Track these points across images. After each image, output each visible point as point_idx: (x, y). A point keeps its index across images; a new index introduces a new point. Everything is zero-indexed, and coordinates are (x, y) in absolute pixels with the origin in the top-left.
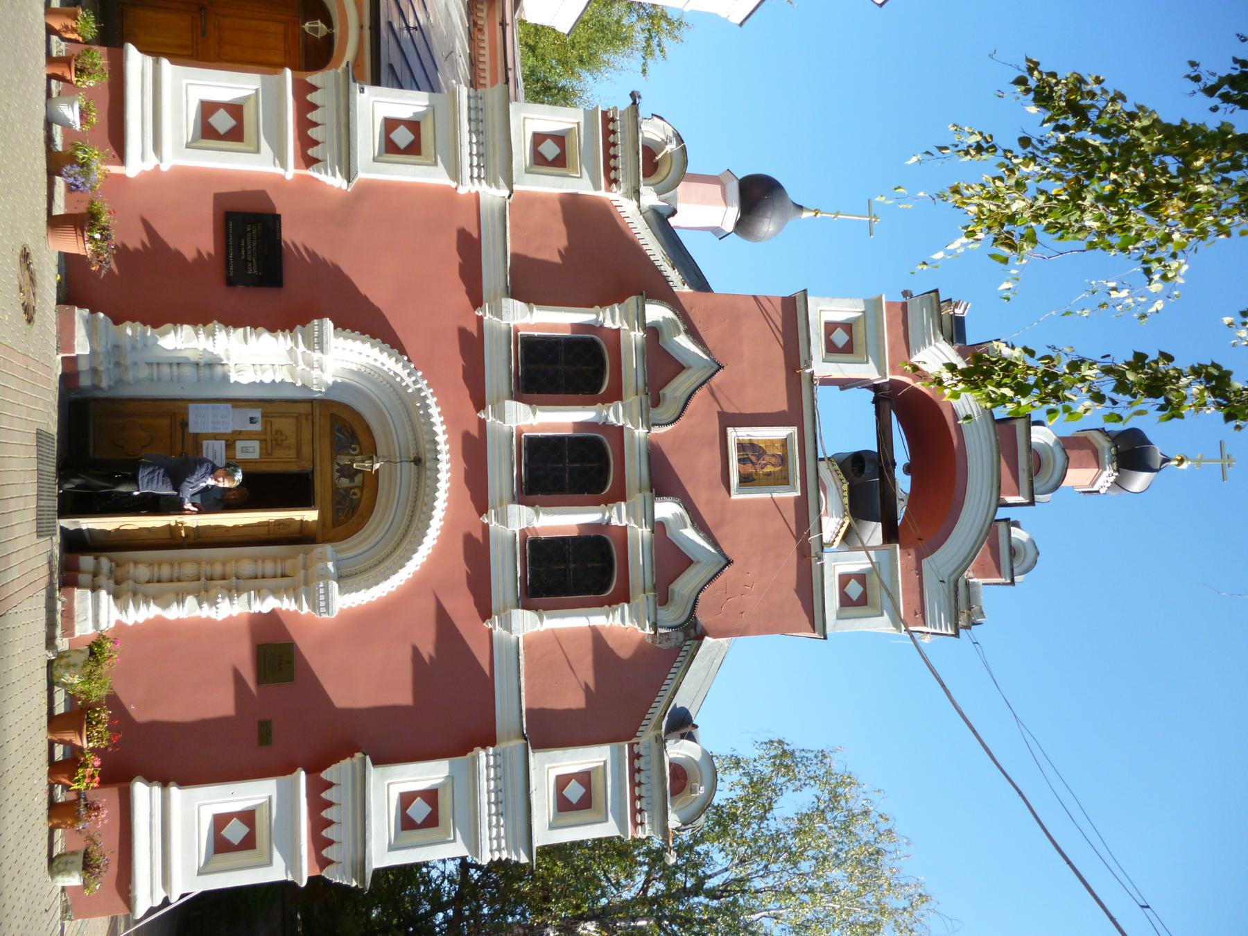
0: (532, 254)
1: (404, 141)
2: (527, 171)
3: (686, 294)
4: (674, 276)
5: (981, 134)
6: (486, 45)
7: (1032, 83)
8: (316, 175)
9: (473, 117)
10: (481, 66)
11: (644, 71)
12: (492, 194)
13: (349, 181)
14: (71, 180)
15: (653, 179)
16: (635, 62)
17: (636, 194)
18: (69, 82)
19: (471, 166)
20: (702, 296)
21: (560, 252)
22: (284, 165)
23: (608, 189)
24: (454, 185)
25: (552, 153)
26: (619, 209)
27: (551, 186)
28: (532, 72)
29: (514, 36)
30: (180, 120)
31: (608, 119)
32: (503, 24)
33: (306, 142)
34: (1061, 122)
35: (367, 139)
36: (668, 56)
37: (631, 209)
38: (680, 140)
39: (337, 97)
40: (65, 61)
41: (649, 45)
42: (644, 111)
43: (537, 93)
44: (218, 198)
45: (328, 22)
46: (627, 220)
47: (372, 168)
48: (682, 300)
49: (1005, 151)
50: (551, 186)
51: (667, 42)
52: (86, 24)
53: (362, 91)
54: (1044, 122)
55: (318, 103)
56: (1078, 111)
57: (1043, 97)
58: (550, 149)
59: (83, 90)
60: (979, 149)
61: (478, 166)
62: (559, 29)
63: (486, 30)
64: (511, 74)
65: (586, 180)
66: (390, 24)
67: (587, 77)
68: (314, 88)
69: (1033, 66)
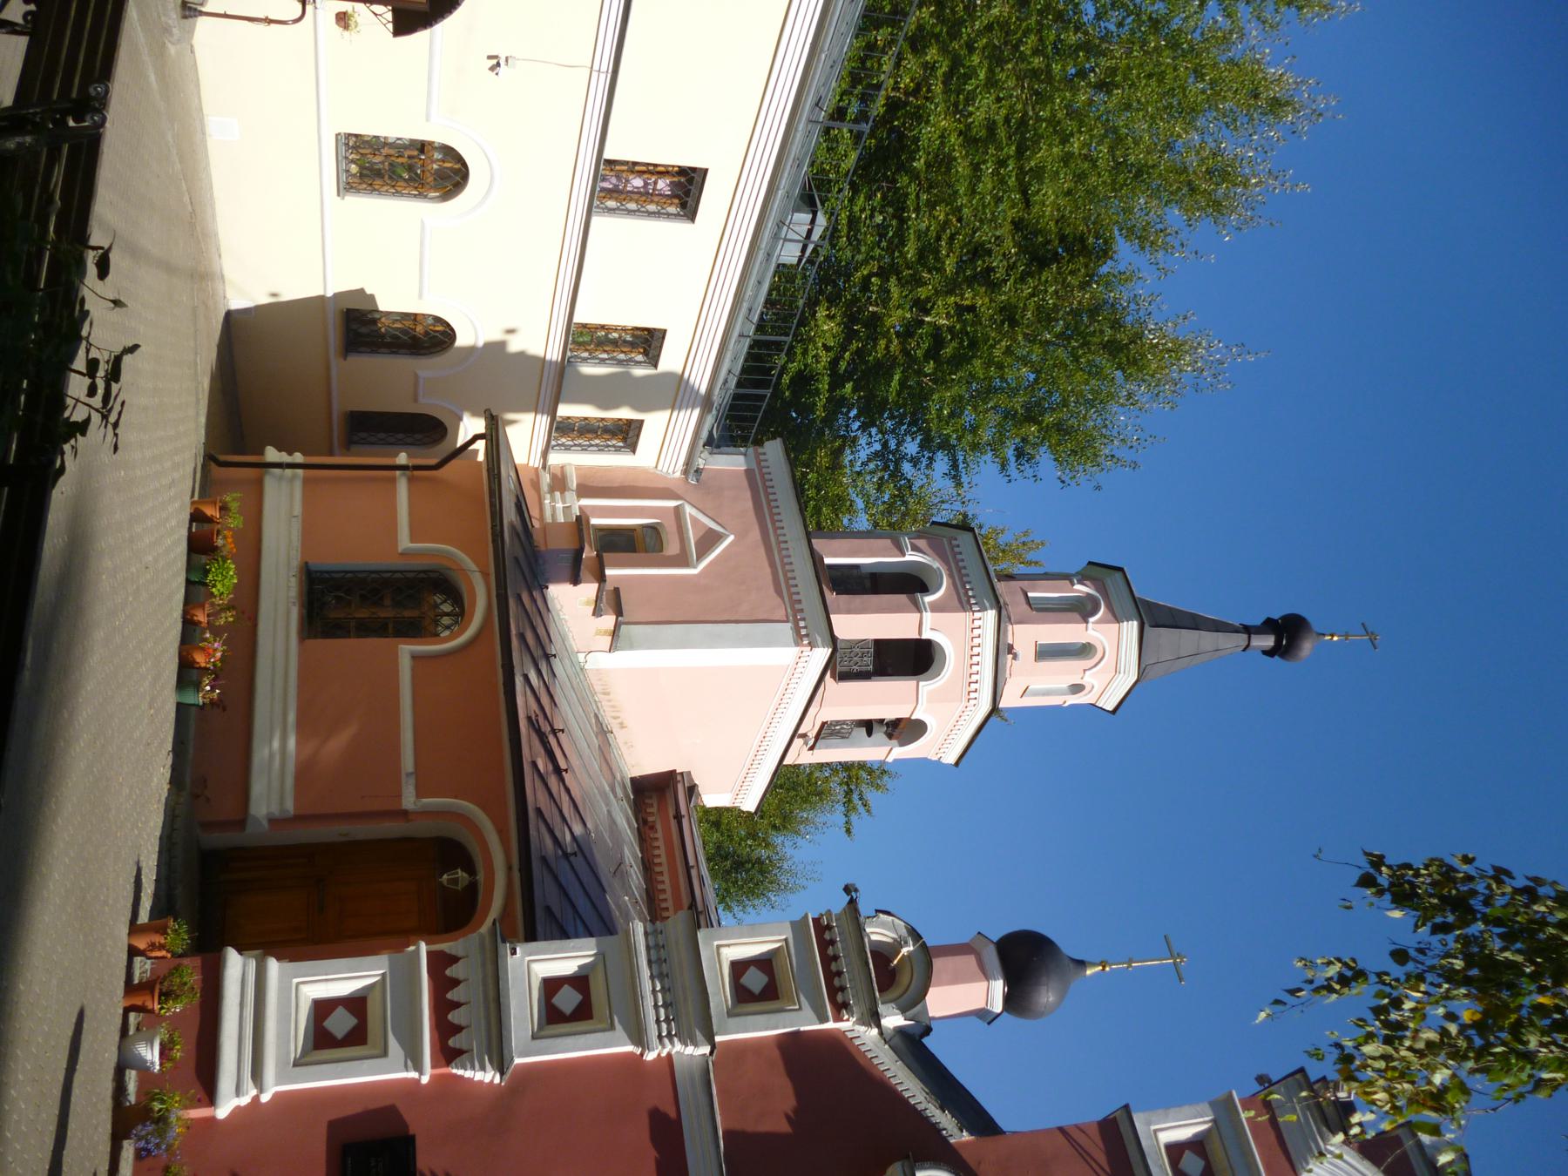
0: (750, 1126)
1: (568, 1006)
2: (730, 1014)
3: (968, 1143)
4: (945, 1120)
5: (1339, 960)
6: (660, 843)
7: (1384, 878)
8: (460, 1072)
9: (653, 958)
10: (657, 869)
11: (848, 831)
12: (692, 1052)
13: (502, 1074)
14: (142, 1144)
15: (894, 992)
16: (838, 816)
17: (874, 1018)
18: (152, 1011)
19: (658, 1021)
20: (990, 1143)
21: (788, 1117)
22: (419, 1068)
23: (838, 1019)
24: (639, 1051)
25: (759, 985)
26: (857, 1042)
27: (761, 1029)
28: (719, 847)
29: (695, 836)
30: (287, 1029)
31: (821, 928)
32: (678, 817)
33: (445, 1030)
34: (1438, 920)
35: (522, 1010)
36: (873, 811)
37: (869, 1036)
38: (915, 935)
39: (484, 965)
40: (147, 987)
41: (850, 801)
42: (865, 908)
43: (728, 872)
44: (334, 1126)
45: (471, 869)
46: (870, 1055)
47: (531, 1053)
48: (965, 1155)
49: (1379, 975)
50: (761, 1029)
51: (871, 795)
52: (178, 935)
53: (514, 952)
54: (1416, 927)
55: (461, 977)
56: (1462, 907)
57: (1403, 895)
58: (755, 980)
59: (164, 1018)
60: (1344, 981)
61: (667, 1020)
62: (745, 808)
63: (659, 826)
64: (694, 872)
65: (808, 1011)
66: (534, 764)
67: (778, 839)
68: (454, 959)
69: (1377, 862)
